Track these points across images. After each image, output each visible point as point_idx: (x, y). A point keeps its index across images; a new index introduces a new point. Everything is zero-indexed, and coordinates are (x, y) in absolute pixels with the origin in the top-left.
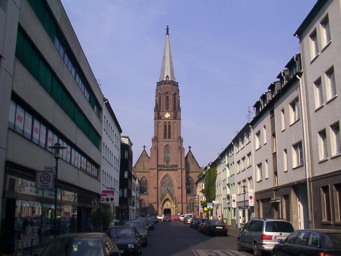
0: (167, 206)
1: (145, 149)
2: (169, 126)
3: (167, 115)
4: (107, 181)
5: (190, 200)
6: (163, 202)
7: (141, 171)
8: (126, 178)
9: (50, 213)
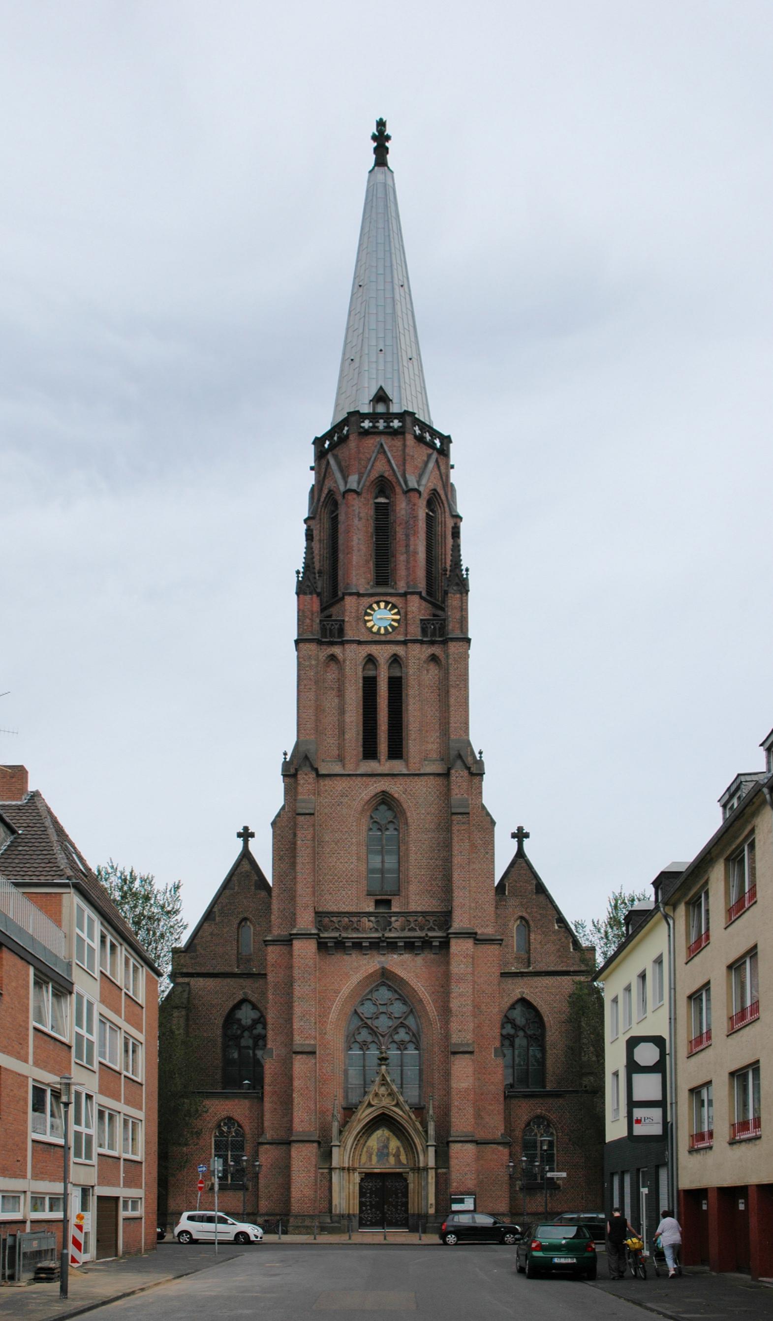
1: (251, 848)
2: (396, 685)
3: (382, 618)
4: (416, 1204)
5: (528, 1124)
6: (355, 1133)
7: (227, 969)
8: (451, 1208)
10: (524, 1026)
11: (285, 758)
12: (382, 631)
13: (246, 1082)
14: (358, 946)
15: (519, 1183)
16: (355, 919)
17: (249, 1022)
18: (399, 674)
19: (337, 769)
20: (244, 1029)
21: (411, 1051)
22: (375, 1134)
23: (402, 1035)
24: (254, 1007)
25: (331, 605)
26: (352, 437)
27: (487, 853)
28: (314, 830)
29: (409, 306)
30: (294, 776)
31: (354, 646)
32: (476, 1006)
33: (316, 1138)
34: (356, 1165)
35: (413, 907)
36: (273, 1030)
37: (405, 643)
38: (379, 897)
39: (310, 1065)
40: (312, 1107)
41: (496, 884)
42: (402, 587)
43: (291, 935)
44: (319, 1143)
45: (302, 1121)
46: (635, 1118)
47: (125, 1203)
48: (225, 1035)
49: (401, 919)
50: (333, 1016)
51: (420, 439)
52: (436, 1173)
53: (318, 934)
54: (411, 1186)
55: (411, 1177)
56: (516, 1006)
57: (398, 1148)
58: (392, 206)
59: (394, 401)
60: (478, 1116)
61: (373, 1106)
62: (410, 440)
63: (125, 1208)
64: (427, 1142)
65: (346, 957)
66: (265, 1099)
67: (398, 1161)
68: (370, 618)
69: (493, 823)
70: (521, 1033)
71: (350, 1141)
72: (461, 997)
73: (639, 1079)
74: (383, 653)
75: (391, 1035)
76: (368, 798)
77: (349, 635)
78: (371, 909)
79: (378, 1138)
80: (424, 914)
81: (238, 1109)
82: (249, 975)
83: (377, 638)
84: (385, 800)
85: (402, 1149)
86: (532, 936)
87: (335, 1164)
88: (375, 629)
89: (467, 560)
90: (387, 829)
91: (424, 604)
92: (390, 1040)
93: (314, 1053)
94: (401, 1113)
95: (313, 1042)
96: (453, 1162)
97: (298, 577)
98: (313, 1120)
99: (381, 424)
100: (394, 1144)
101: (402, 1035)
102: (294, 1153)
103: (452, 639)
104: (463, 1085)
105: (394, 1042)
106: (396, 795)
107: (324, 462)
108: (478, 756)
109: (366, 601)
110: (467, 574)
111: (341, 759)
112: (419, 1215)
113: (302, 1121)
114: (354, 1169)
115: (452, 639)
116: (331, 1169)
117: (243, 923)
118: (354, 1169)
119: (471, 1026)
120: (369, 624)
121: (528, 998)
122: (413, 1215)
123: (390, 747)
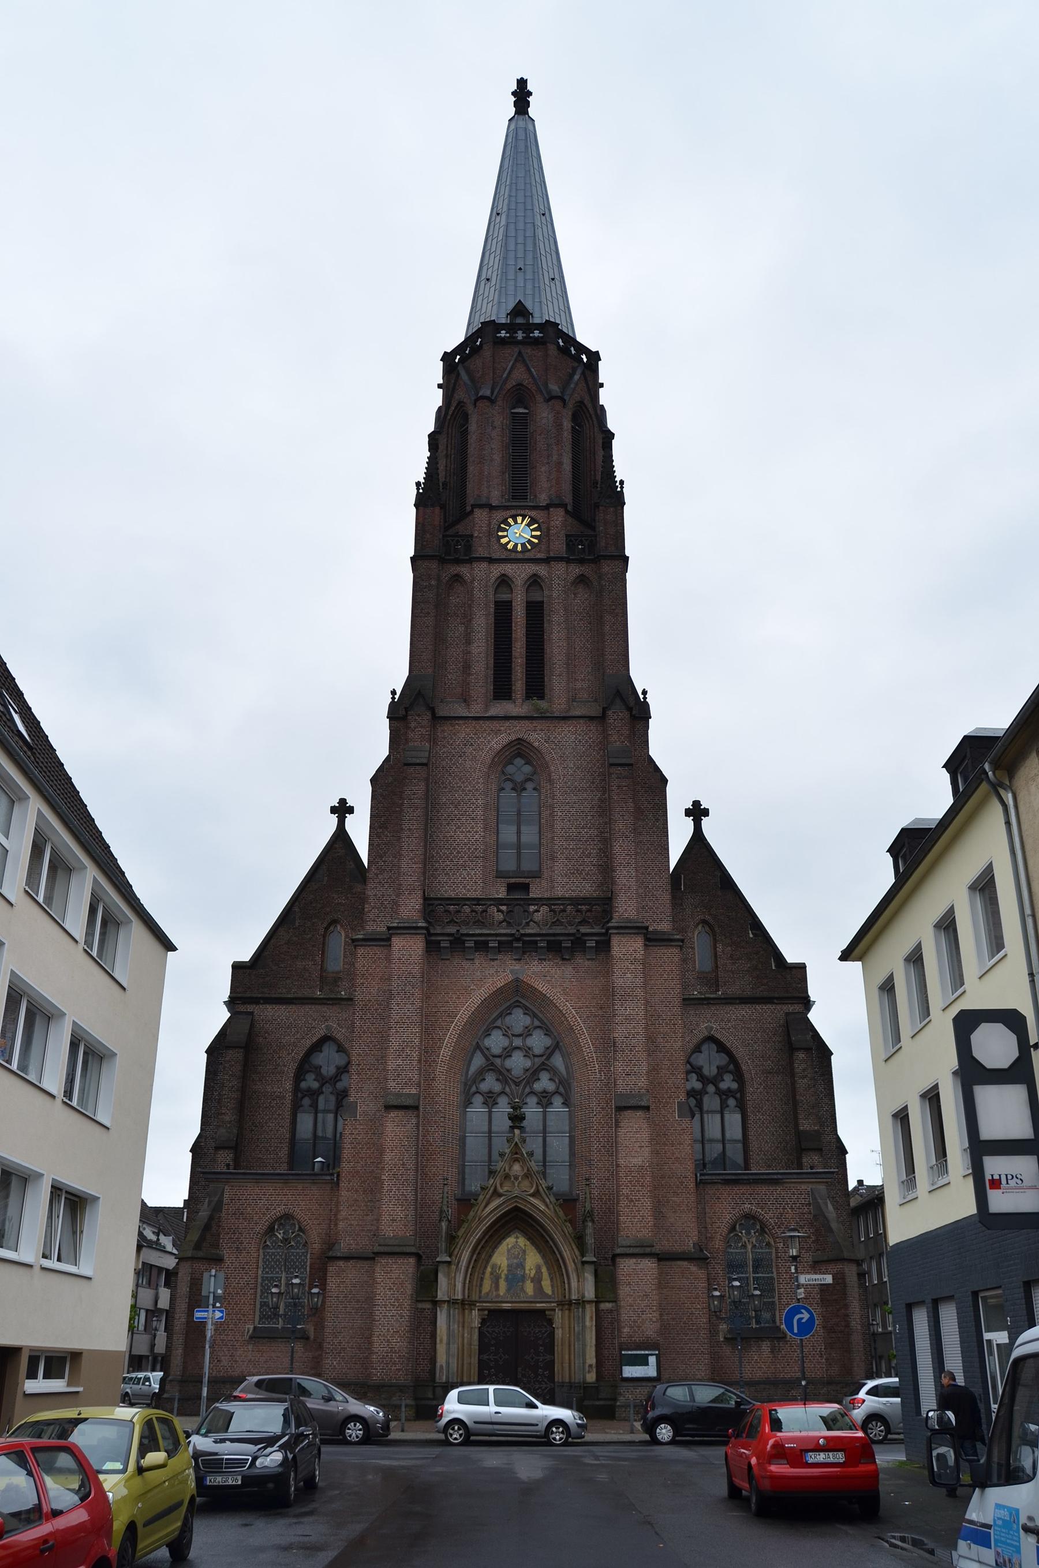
0: (515, 1278)
2: (536, 612)
3: (519, 533)
4: (566, 1365)
5: (733, 1229)
6: (473, 1240)
9: (840, 1403)
10: (715, 1077)
11: (393, 698)
12: (519, 548)
13: (319, 1159)
14: (482, 946)
15: (723, 1327)
16: (480, 908)
17: (332, 1070)
18: (540, 599)
19: (462, 712)
20: (323, 1081)
21: (557, 1106)
22: (505, 1243)
23: (544, 1083)
24: (341, 1049)
25: (458, 521)
26: (485, 347)
27: (657, 820)
28: (427, 786)
29: (550, 233)
30: (404, 718)
31: (484, 565)
32: (650, 1039)
33: (413, 1250)
34: (475, 1297)
35: (559, 892)
36: (359, 1074)
37: (547, 561)
38: (513, 880)
39: (408, 1127)
40: (411, 1197)
41: (672, 865)
42: (543, 499)
43: (389, 928)
44: (418, 1257)
45: (393, 1220)
46: (988, 1177)
47: (34, 1361)
48: (296, 1088)
49: (544, 909)
50: (445, 1053)
51: (565, 351)
53: (426, 928)
54: (559, 1333)
55: (559, 1318)
56: (705, 1047)
57: (538, 1268)
58: (534, 148)
59: (535, 315)
60: (658, 1213)
61: (500, 1195)
62: (552, 350)
63: (32, 1375)
65: (466, 964)
66: (342, 1185)
67: (539, 1289)
68: (505, 533)
69: (664, 781)
70: (711, 1088)
72: (630, 1020)
73: (987, 1096)
74: (519, 573)
75: (528, 1083)
76: (499, 747)
77: (480, 551)
78: (502, 893)
79: (509, 1251)
80: (576, 901)
81: (302, 1202)
82: (337, 1001)
83: (513, 556)
84: (519, 750)
85: (544, 1270)
86: (720, 948)
87: (441, 1294)
88: (510, 546)
89: (621, 470)
90: (525, 789)
91: (570, 520)
92: (527, 1090)
93: (417, 1108)
94: (542, 1207)
95: (414, 1091)
96: (623, 1291)
97: (418, 489)
98: (410, 1218)
99: (520, 335)
100: (533, 1259)
101: (544, 1083)
102: (379, 1275)
103: (605, 557)
104: (635, 1161)
105: (533, 1093)
106: (536, 744)
107: (453, 376)
108: (641, 696)
109: (499, 515)
110: (622, 488)
111: (466, 700)
112: (571, 1385)
113: (393, 1220)
115: (605, 557)
116: (436, 1303)
117: (332, 928)
118: (472, 1304)
119: (644, 1068)
120: (504, 541)
121: (718, 1036)
122: (562, 1385)
123: (528, 635)
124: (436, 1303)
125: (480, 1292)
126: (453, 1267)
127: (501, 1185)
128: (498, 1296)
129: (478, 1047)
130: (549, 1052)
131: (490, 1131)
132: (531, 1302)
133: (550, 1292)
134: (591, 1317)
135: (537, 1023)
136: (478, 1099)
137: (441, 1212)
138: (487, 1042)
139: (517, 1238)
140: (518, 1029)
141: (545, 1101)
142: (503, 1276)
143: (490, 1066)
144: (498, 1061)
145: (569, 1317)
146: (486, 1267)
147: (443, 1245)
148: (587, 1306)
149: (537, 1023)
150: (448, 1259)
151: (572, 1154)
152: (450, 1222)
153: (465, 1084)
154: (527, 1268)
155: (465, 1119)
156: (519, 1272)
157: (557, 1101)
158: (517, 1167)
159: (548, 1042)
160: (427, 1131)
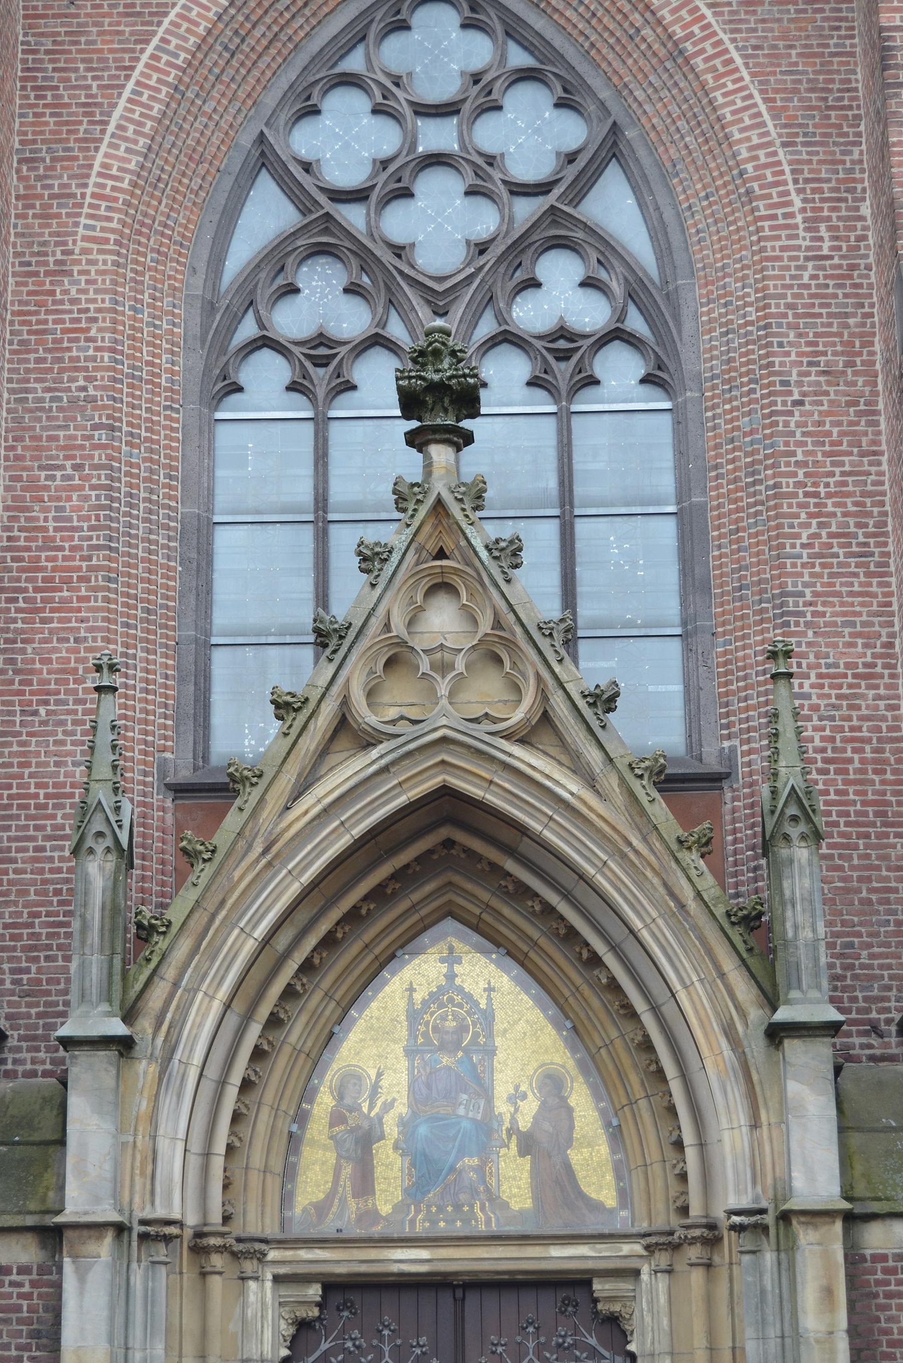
23: (560, 296)
34: (256, 1220)
52: (854, 1260)
55: (654, 1308)
57: (552, 1085)
61: (367, 740)
64: (771, 999)
71: (204, 1016)
79: (414, 1016)
87: (83, 1195)
94: (569, 786)
101: (560, 296)
105: (508, 338)
114: (247, 1251)
118: (247, 1251)
124: (53, 1236)
125: (286, 1199)
126: (144, 1069)
127: (371, 694)
128: (373, 1215)
129: (265, 158)
130: (579, 174)
131: (321, 501)
132: (524, 1239)
133: (608, 1197)
134: (828, 1292)
135: (519, 58)
136: (266, 375)
137: (85, 810)
138: (305, 141)
139: (452, 958)
140: (439, 191)
141: (563, 370)
142: (391, 1129)
143: (321, 232)
144: (354, 217)
145: (709, 1300)
146: (307, 1094)
147: (90, 964)
148: (807, 1237)
149: (519, 58)
150: (118, 1028)
151: (693, 581)
152: (126, 856)
153: (210, 308)
154: (502, 1089)
155: (209, 449)
156: (466, 1110)
157: (620, 369)
158: (443, 621)
159: (572, 132)
160: (33, 486)
